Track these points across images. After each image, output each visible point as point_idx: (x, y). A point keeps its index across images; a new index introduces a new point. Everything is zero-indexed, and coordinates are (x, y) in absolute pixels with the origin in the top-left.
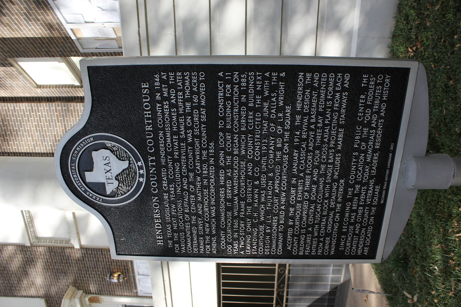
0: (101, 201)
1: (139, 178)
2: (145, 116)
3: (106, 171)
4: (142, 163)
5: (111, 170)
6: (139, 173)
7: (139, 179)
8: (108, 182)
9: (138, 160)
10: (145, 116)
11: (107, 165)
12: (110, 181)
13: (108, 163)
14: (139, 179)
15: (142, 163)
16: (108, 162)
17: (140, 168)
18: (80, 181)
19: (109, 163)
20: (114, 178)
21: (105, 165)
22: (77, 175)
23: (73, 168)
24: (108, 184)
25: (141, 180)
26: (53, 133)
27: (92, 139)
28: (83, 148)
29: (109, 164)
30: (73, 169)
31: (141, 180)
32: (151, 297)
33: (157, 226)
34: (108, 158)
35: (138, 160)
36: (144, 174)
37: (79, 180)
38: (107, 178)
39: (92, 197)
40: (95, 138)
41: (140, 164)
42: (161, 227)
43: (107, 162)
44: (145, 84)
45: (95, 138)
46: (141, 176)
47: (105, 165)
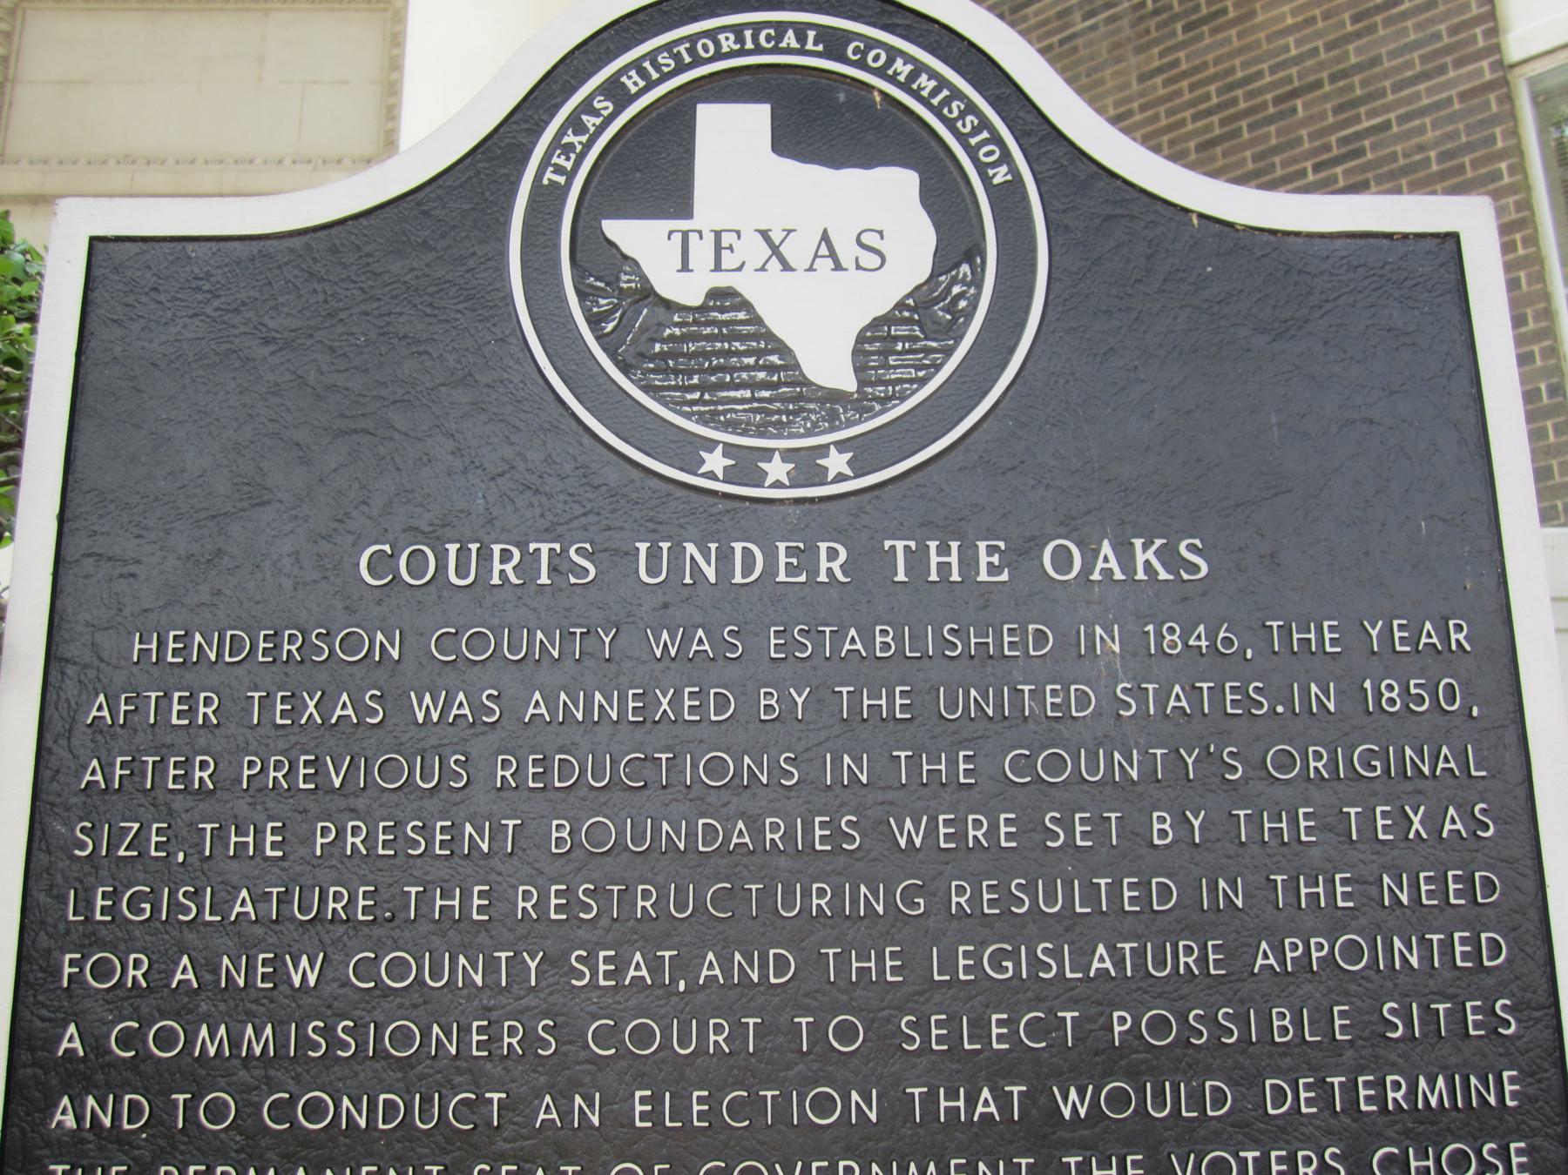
0: (549, 175)
1: (788, 455)
2: (933, 545)
3: (776, 237)
4: (841, 478)
5: (786, 267)
6: (767, 454)
7: (777, 456)
8: (693, 237)
9: (865, 454)
10: (933, 545)
11: (824, 250)
12: (702, 252)
13: (833, 254)
14: (777, 456)
15: (711, 476)
16: (710, 238)
17: (807, 467)
18: (690, 66)
19: (838, 267)
20: (722, 281)
21: (825, 237)
22: (732, 54)
23: (790, 39)
24: (677, 237)
25: (715, 461)
26: (1383, 51)
27: (1001, 175)
28: (937, 111)
29: (829, 263)
30: (779, 37)
31: (715, 461)
32: (1554, 599)
33: (748, 555)
34: (871, 260)
35: (865, 454)
36: (760, 485)
37: (698, 62)
38: (727, 239)
39: (574, 123)
40: (1008, 199)
41: (837, 462)
42: (738, 579)
43: (847, 251)
44: (995, 559)
45: (1008, 199)
46: (746, 466)
47: (825, 237)
